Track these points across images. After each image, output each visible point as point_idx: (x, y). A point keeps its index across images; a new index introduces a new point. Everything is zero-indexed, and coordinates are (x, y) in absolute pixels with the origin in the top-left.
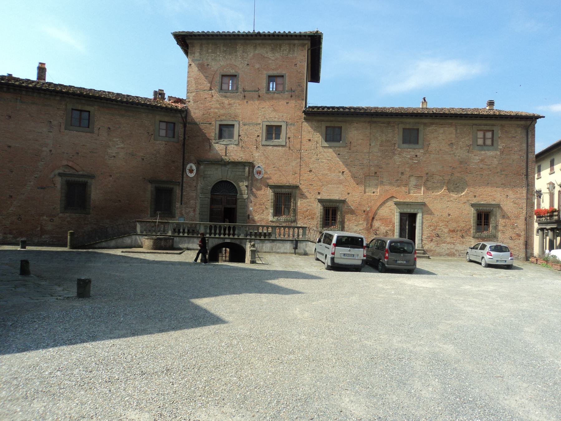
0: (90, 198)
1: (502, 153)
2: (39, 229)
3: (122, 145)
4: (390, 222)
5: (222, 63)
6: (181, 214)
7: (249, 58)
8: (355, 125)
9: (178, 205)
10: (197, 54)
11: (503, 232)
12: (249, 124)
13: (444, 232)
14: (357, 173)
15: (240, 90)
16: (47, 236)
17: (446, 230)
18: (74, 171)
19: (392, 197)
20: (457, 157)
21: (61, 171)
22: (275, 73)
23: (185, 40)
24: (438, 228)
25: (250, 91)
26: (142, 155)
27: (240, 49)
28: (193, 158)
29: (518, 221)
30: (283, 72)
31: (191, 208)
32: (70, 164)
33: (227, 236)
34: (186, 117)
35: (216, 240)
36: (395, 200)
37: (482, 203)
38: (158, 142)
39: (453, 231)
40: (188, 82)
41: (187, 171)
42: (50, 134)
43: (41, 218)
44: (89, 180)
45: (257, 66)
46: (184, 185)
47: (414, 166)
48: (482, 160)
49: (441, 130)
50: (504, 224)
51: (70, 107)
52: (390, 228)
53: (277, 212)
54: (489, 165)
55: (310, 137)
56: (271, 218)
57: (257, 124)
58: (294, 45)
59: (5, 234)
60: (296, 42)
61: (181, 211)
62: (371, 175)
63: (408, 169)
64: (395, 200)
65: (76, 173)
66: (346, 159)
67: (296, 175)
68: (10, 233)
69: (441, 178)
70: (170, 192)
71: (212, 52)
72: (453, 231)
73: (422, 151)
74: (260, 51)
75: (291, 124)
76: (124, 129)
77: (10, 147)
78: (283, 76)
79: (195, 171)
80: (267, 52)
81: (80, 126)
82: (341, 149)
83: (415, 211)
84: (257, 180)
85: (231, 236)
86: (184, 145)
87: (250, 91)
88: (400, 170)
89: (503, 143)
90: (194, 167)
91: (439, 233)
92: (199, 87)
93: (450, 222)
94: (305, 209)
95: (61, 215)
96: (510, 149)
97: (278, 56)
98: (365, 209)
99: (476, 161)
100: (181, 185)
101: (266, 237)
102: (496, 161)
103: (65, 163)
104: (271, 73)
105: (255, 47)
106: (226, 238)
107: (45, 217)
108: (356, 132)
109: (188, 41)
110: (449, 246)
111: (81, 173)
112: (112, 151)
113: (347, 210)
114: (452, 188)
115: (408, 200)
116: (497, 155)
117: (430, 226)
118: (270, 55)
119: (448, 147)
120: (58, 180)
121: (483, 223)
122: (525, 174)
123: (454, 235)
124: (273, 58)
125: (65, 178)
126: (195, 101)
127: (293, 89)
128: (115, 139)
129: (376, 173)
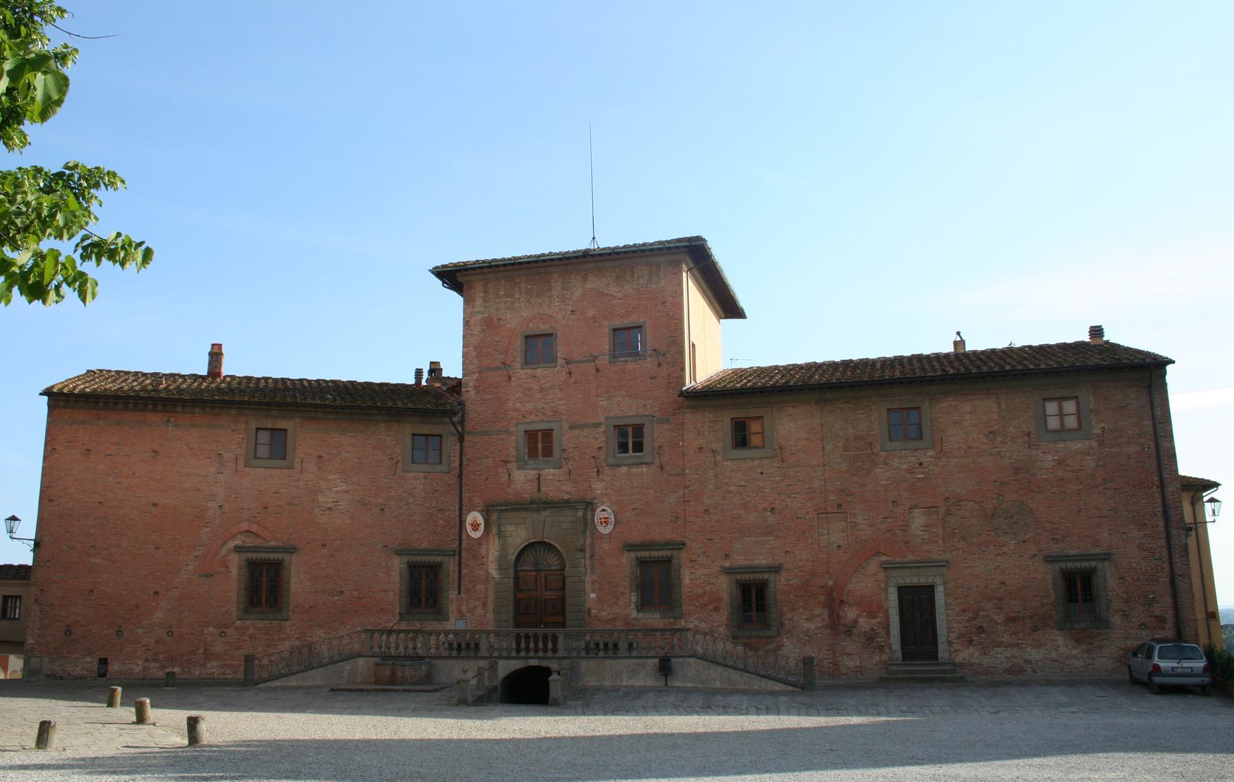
1: (1101, 443)
2: (201, 650)
3: (344, 487)
5: (525, 314)
6: (460, 612)
8: (790, 410)
9: (453, 594)
12: (581, 427)
15: (561, 361)
16: (215, 664)
17: (999, 618)
18: (260, 541)
19: (878, 553)
21: (238, 542)
22: (626, 322)
23: (452, 276)
25: (579, 362)
26: (382, 501)
27: (557, 284)
31: (478, 599)
32: (254, 528)
33: (532, 654)
34: (462, 422)
35: (513, 662)
36: (884, 558)
37: (1072, 552)
38: (409, 475)
39: (1014, 619)
41: (469, 528)
42: (221, 476)
43: (206, 630)
44: (287, 557)
45: (590, 312)
46: (464, 555)
48: (1060, 463)
49: (967, 407)
50: (1125, 596)
51: (253, 425)
53: (643, 606)
54: (1077, 471)
56: (634, 614)
57: (597, 425)
58: (658, 266)
59: (147, 661)
60: (661, 259)
61: (460, 605)
63: (906, 494)
64: (884, 558)
68: (156, 660)
70: (435, 568)
72: (1014, 619)
73: (931, 453)
74: (593, 283)
76: (347, 455)
77: (155, 505)
79: (482, 526)
80: (607, 285)
81: (427, 463)
82: (766, 462)
83: (930, 580)
84: (602, 536)
86: (460, 476)
87: (579, 362)
90: (480, 520)
94: (699, 591)
95: (238, 623)
99: (1047, 465)
101: (607, 648)
102: (1090, 463)
103: (244, 526)
104: (618, 323)
105: (585, 279)
107: (211, 629)
109: (460, 279)
111: (272, 543)
112: (326, 499)
115: (910, 557)
117: (964, 611)
118: (614, 289)
119: (986, 440)
120: (235, 562)
121: (1080, 598)
124: (619, 295)
125: (245, 556)
128: (331, 477)
129: (839, 506)
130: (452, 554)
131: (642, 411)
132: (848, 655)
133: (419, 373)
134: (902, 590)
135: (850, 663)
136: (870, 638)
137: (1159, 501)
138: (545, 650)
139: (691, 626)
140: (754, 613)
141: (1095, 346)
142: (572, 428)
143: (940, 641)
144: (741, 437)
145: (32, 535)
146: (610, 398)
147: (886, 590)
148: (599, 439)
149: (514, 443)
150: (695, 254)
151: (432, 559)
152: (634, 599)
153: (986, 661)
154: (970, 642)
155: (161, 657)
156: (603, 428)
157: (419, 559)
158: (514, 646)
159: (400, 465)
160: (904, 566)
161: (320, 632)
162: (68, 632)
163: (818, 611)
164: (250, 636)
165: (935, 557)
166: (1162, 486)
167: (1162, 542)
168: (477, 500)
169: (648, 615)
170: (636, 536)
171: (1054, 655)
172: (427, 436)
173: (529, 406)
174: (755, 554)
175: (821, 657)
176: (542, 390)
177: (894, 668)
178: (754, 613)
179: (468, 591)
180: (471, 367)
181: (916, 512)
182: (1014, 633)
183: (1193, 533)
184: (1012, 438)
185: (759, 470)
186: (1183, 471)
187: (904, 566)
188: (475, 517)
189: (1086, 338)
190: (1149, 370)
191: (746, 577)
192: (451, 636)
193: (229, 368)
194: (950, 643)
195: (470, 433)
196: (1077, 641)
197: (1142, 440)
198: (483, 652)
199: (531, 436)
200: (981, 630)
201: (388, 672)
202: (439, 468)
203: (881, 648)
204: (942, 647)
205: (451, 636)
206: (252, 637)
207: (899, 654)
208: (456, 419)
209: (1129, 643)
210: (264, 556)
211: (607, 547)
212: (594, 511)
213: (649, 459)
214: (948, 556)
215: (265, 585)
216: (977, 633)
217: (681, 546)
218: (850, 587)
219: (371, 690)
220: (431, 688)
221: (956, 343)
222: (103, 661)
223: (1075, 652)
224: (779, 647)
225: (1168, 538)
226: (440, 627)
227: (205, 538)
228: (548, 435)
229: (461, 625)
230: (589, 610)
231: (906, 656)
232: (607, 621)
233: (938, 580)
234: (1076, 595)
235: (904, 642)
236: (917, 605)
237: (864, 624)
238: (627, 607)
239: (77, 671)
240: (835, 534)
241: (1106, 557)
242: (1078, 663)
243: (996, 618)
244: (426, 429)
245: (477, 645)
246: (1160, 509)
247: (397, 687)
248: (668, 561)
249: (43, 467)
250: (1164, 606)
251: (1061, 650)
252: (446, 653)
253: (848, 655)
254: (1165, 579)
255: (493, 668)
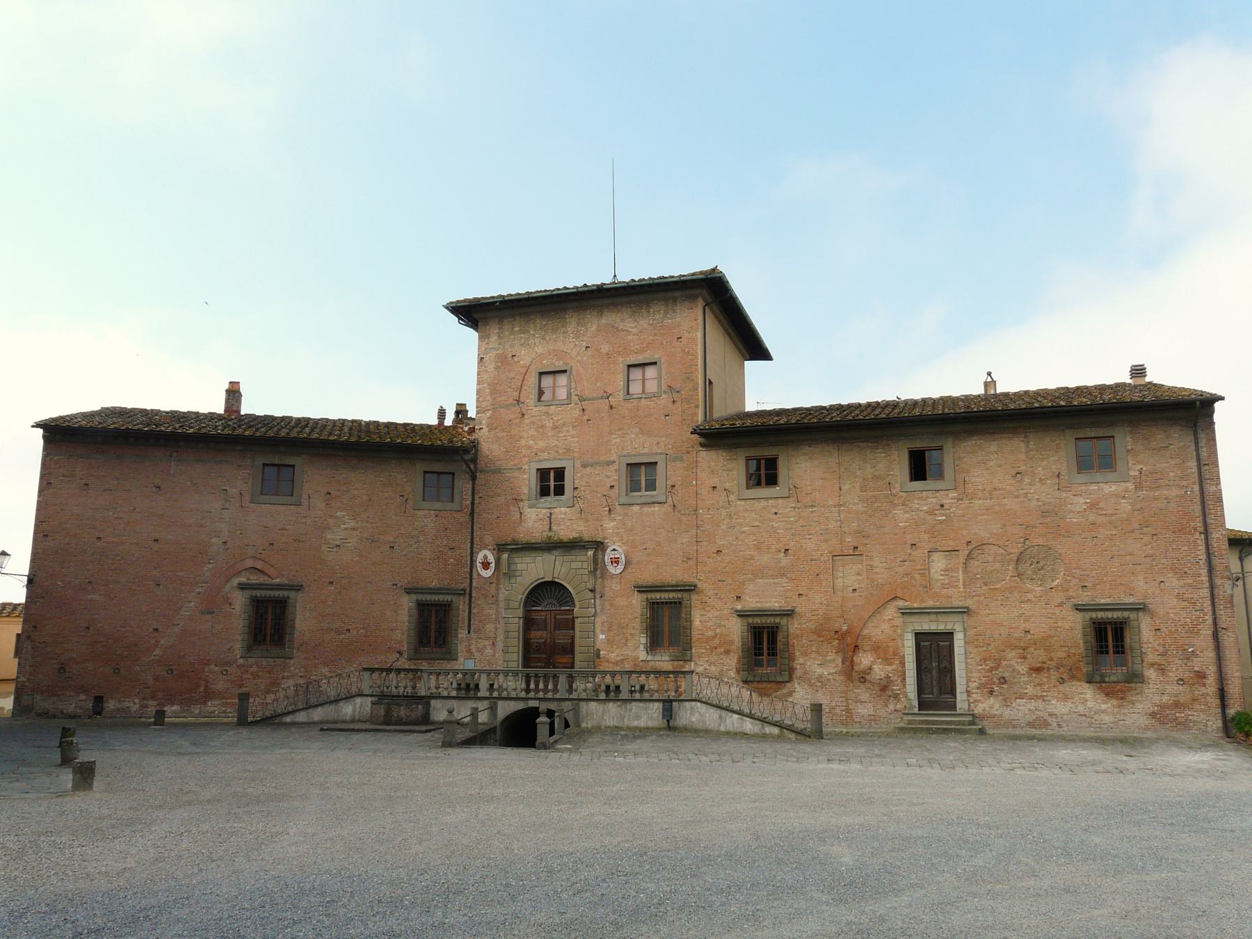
0: (293, 627)
1: (1139, 487)
2: (202, 689)
3: (353, 524)
4: (895, 654)
5: (539, 350)
6: (469, 651)
7: (589, 334)
9: (463, 634)
10: (494, 338)
11: (1162, 670)
12: (592, 465)
13: (1019, 673)
14: (815, 551)
17: (1022, 668)
19: (895, 598)
20: (1035, 502)
21: (243, 580)
22: (640, 359)
23: (471, 313)
24: (1004, 663)
25: (593, 399)
26: (391, 539)
28: (488, 539)
29: (1195, 641)
30: (656, 357)
32: (259, 565)
33: (532, 694)
34: (474, 460)
36: (901, 603)
37: (1103, 601)
38: (419, 513)
39: (1038, 670)
40: (478, 392)
41: (479, 565)
44: (292, 594)
45: (605, 348)
47: (939, 527)
48: (1093, 506)
52: (894, 667)
53: (654, 644)
54: (1111, 515)
55: (714, 481)
56: (643, 655)
59: (144, 699)
60: (678, 294)
62: (846, 552)
63: (925, 537)
64: (901, 603)
65: (269, 581)
66: (792, 523)
67: (690, 563)
68: (153, 698)
69: (1001, 551)
70: (445, 608)
71: (521, 332)
72: (1038, 670)
73: (952, 494)
75: (675, 460)
76: (356, 492)
78: (655, 363)
79: (493, 565)
80: (623, 321)
81: (438, 500)
82: (780, 501)
83: (949, 627)
85: (541, 695)
86: (472, 514)
88: (910, 538)
89: (1140, 463)
90: (491, 558)
91: (1007, 675)
92: (498, 399)
93: (1032, 649)
94: (710, 633)
95: (241, 661)
96: (1158, 476)
97: (645, 326)
98: (837, 626)
100: (467, 593)
102: (1125, 506)
104: (633, 359)
106: (550, 699)
107: (212, 667)
108: (808, 464)
109: (476, 316)
110: (1032, 705)
111: (277, 581)
113: (798, 632)
114: (1030, 572)
115: (930, 603)
116: (1126, 490)
117: (985, 660)
121: (1111, 651)
122: (1202, 529)
123: (1043, 677)
126: (491, 428)
127: (677, 386)
128: (339, 514)
129: (856, 548)
130: (462, 593)
131: (655, 449)
132: (861, 702)
133: (442, 414)
134: (919, 636)
135: (863, 711)
136: (884, 687)
137: (1202, 548)
138: (546, 690)
139: (700, 669)
140: (765, 657)
141: (1136, 387)
142: (584, 466)
143: (958, 691)
144: (919, 469)
145: (26, 570)
146: (623, 436)
147: (902, 636)
148: (615, 476)
149: (528, 482)
150: (712, 291)
151: (441, 598)
152: (643, 640)
153: (1007, 713)
154: (991, 693)
155: (160, 695)
156: (616, 466)
157: (429, 597)
158: (524, 685)
159: (411, 503)
160: (921, 612)
161: (325, 670)
162: (62, 669)
163: (831, 656)
164: (252, 674)
165: (956, 603)
166: (1206, 532)
167: (1205, 592)
168: (488, 539)
169: (658, 658)
170: (647, 578)
171: (1081, 709)
172: (439, 473)
173: (542, 444)
174: (766, 596)
175: (833, 704)
176: (555, 428)
177: (910, 718)
178: (765, 657)
179: (477, 631)
180: (484, 404)
181: (936, 556)
182: (1040, 685)
183: (1240, 583)
184: (1041, 480)
185: (774, 510)
186: (1229, 525)
187: (921, 612)
188: (487, 554)
189: (1126, 378)
190: (1191, 413)
191: (758, 620)
192: (460, 676)
193: (248, 407)
194: (969, 693)
195: (482, 471)
196: (1107, 695)
197: (1184, 483)
198: (483, 693)
199: (543, 474)
200: (1003, 681)
201: (382, 712)
202: (450, 506)
203: (896, 697)
204: (961, 697)
205: (460, 676)
206: (255, 676)
207: (916, 703)
208: (467, 457)
209: (1165, 699)
210: (272, 593)
211: (616, 587)
212: (604, 551)
213: (662, 499)
214: (969, 603)
215: (269, 621)
216: (996, 684)
217: (691, 589)
218: (865, 632)
219: (379, 730)
220: (424, 728)
221: (986, 384)
222: (99, 700)
223: (1104, 707)
224: (790, 694)
225: (1212, 587)
226: (449, 667)
227: (208, 574)
228: (560, 473)
229: (470, 665)
230: (599, 651)
231: (922, 706)
232: (616, 663)
233: (958, 627)
234: (1107, 646)
235: (920, 691)
236: (934, 653)
237: (879, 671)
238: (636, 650)
239: (71, 709)
240: (850, 577)
241: (1141, 608)
242: (1107, 719)
243: (1019, 668)
244: (437, 467)
245: (477, 686)
246: (1204, 557)
247: (388, 728)
248: (678, 604)
249: (39, 502)
250: (1205, 660)
251: (1090, 704)
252: (454, 693)
253: (861, 702)
254: (1207, 632)
255: (493, 709)
